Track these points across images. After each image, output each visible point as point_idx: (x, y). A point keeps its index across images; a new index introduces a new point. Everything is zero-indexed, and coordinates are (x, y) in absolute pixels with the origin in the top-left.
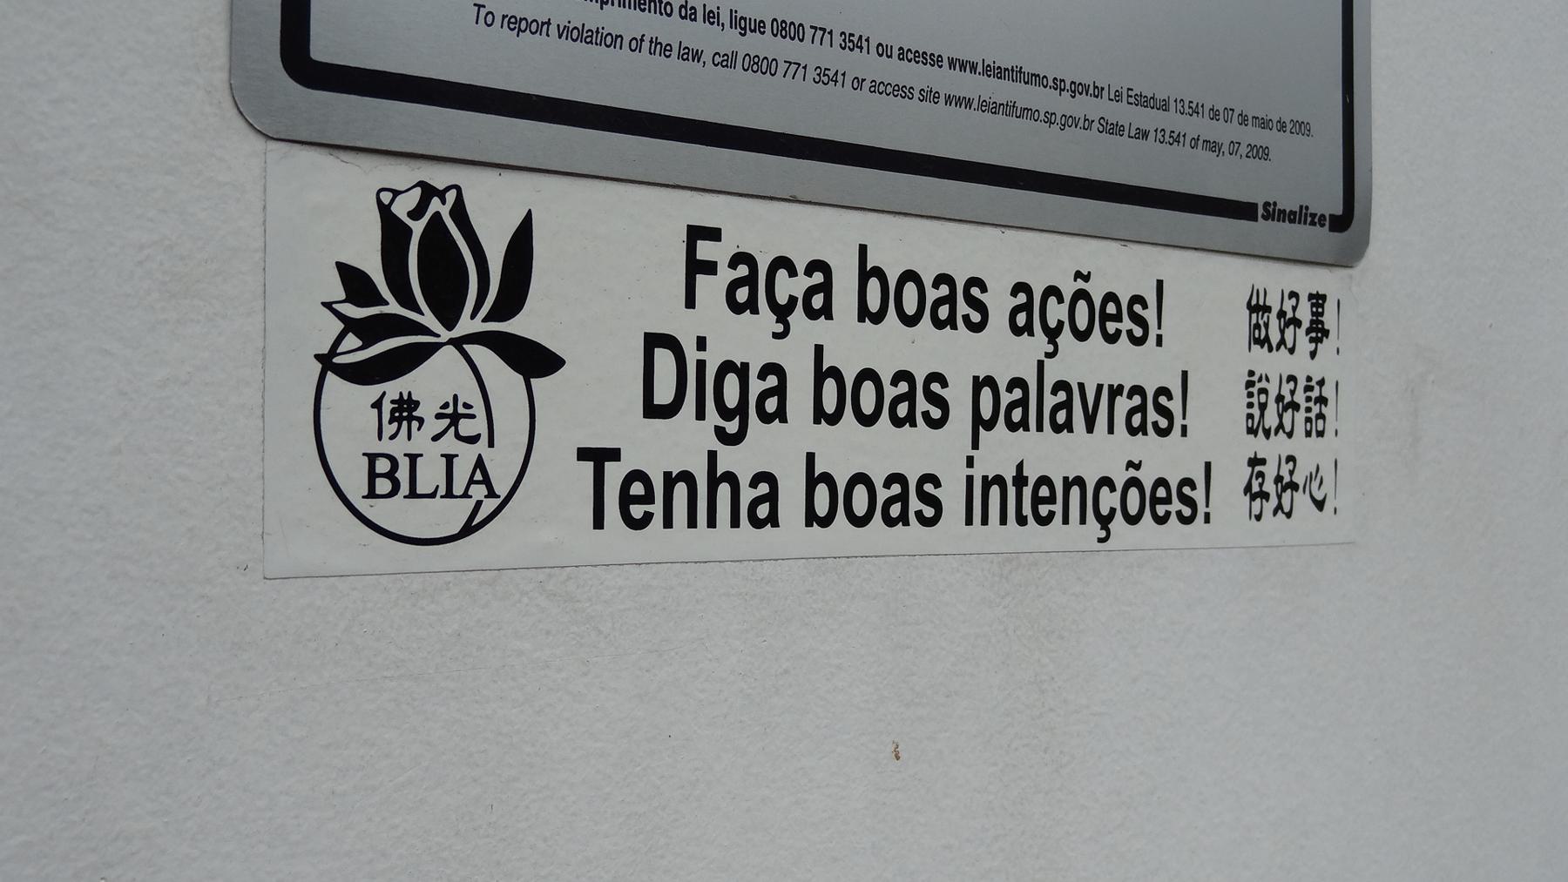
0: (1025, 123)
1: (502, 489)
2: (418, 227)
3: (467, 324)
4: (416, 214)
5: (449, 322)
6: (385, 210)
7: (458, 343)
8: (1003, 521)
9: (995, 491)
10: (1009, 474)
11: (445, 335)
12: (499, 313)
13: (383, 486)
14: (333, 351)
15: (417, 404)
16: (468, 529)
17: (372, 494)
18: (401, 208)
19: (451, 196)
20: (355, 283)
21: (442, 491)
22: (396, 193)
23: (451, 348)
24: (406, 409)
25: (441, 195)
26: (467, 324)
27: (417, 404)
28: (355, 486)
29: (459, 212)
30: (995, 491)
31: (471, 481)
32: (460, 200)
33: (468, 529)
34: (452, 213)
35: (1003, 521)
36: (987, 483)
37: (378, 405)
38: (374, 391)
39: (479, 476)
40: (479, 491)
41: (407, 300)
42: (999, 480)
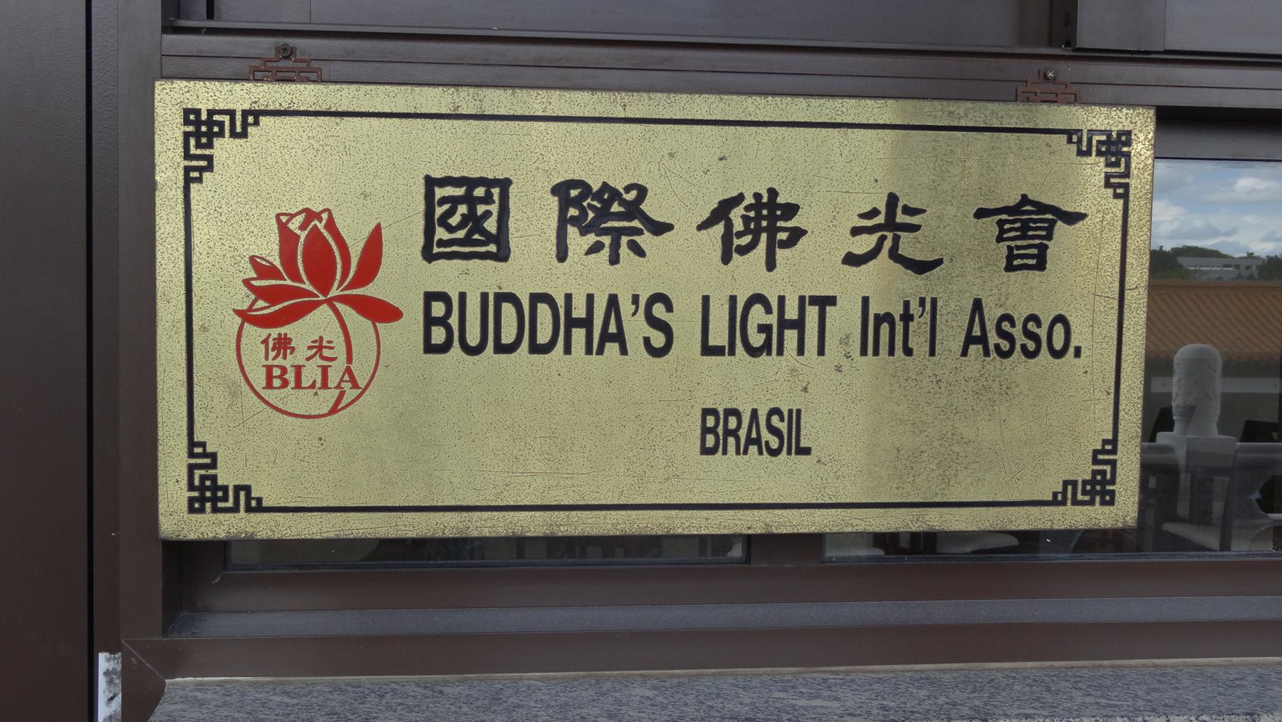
0: (571, 366)
1: (362, 383)
2: (303, 235)
3: (334, 292)
4: (302, 227)
5: (325, 293)
6: (283, 228)
7: (330, 302)
8: (891, 353)
9: (885, 328)
10: (897, 311)
11: (322, 298)
12: (356, 283)
13: (277, 383)
14: (250, 309)
15: (290, 340)
16: (334, 411)
17: (269, 385)
18: (294, 225)
19: (325, 216)
20: (263, 270)
21: (318, 385)
22: (292, 216)
23: (325, 307)
24: (283, 345)
25: (318, 216)
26: (334, 292)
27: (290, 340)
28: (259, 379)
29: (331, 225)
30: (885, 328)
31: (342, 380)
32: (331, 219)
33: (334, 411)
34: (326, 227)
35: (891, 353)
36: (879, 319)
37: (265, 342)
38: (264, 332)
39: (347, 378)
40: (347, 386)
41: (296, 277)
42: (888, 318)
